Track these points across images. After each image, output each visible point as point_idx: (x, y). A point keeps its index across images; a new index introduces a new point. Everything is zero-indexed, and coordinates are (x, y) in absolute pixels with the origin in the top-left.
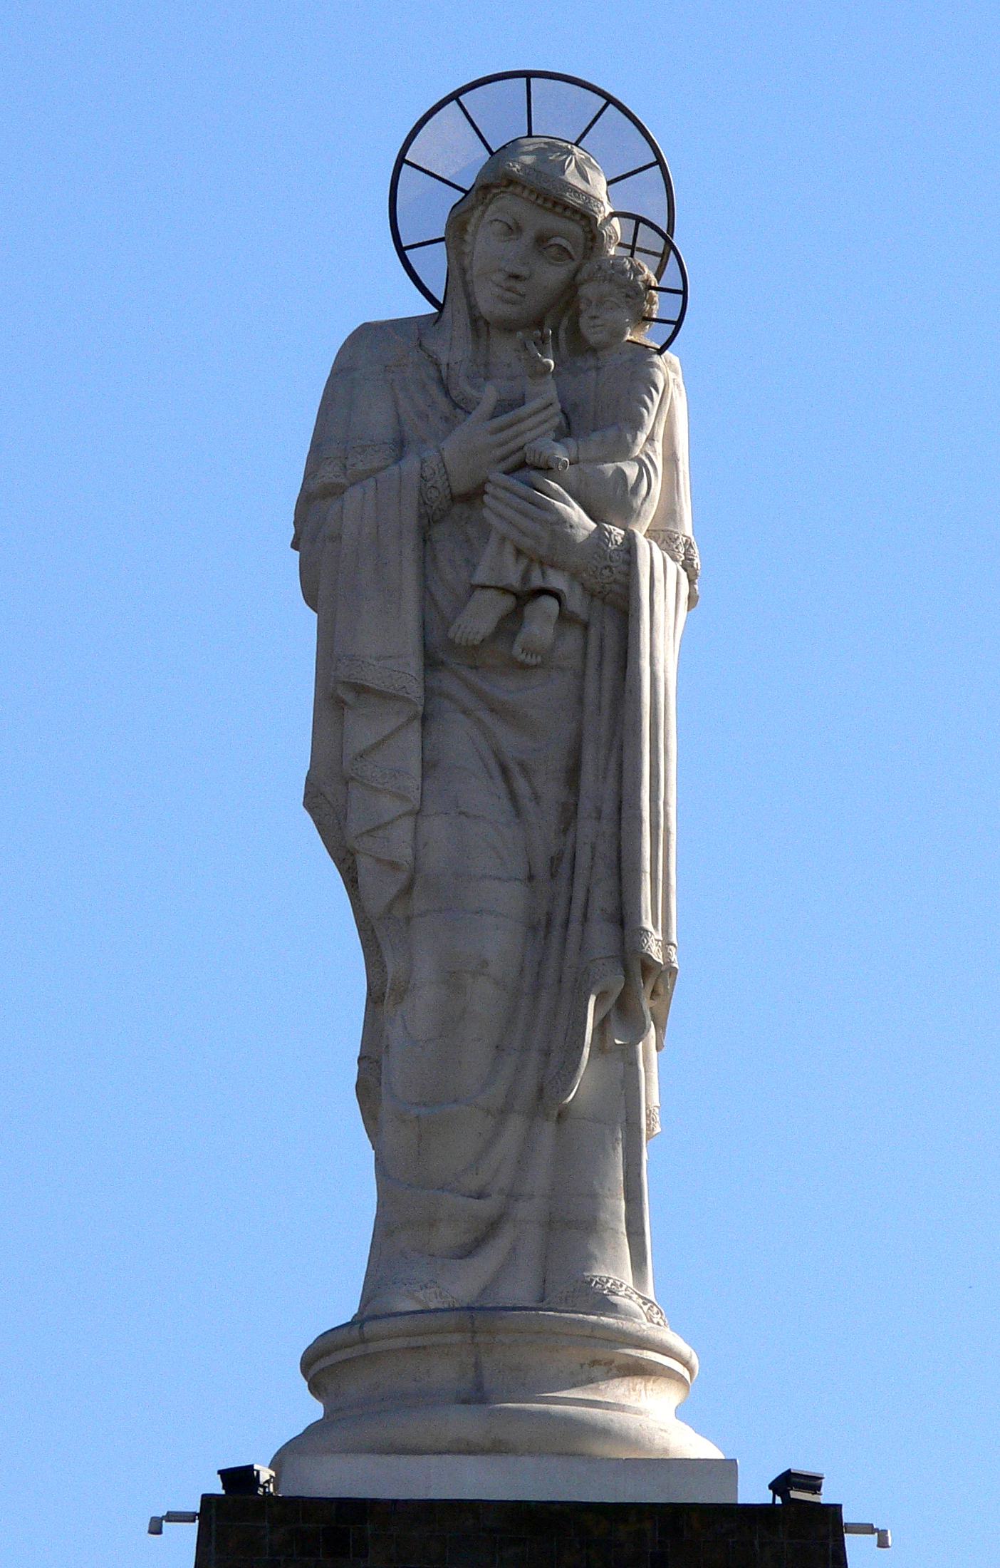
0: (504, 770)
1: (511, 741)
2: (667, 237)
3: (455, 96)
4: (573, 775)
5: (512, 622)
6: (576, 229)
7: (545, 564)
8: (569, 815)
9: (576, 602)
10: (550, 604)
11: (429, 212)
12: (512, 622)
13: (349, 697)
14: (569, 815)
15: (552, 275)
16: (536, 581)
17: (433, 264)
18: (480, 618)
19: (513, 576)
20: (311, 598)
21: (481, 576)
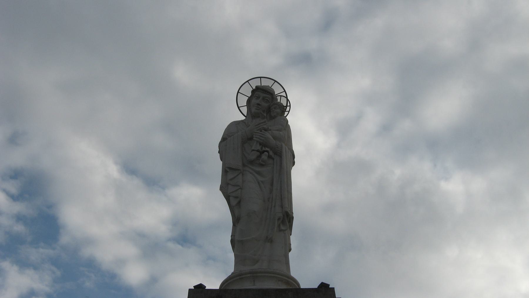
0: (259, 183)
1: (260, 178)
2: (287, 97)
3: (248, 81)
4: (272, 184)
5: (259, 157)
6: (270, 96)
7: (265, 146)
8: (271, 191)
9: (271, 153)
10: (266, 153)
11: (243, 101)
12: (259, 157)
13: (228, 170)
14: (271, 191)
15: (265, 105)
16: (264, 149)
17: (245, 110)
18: (253, 156)
19: (259, 147)
20: (221, 160)
21: (253, 148)
